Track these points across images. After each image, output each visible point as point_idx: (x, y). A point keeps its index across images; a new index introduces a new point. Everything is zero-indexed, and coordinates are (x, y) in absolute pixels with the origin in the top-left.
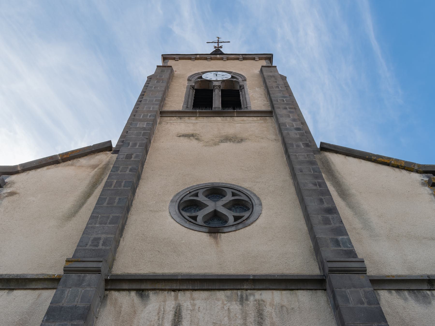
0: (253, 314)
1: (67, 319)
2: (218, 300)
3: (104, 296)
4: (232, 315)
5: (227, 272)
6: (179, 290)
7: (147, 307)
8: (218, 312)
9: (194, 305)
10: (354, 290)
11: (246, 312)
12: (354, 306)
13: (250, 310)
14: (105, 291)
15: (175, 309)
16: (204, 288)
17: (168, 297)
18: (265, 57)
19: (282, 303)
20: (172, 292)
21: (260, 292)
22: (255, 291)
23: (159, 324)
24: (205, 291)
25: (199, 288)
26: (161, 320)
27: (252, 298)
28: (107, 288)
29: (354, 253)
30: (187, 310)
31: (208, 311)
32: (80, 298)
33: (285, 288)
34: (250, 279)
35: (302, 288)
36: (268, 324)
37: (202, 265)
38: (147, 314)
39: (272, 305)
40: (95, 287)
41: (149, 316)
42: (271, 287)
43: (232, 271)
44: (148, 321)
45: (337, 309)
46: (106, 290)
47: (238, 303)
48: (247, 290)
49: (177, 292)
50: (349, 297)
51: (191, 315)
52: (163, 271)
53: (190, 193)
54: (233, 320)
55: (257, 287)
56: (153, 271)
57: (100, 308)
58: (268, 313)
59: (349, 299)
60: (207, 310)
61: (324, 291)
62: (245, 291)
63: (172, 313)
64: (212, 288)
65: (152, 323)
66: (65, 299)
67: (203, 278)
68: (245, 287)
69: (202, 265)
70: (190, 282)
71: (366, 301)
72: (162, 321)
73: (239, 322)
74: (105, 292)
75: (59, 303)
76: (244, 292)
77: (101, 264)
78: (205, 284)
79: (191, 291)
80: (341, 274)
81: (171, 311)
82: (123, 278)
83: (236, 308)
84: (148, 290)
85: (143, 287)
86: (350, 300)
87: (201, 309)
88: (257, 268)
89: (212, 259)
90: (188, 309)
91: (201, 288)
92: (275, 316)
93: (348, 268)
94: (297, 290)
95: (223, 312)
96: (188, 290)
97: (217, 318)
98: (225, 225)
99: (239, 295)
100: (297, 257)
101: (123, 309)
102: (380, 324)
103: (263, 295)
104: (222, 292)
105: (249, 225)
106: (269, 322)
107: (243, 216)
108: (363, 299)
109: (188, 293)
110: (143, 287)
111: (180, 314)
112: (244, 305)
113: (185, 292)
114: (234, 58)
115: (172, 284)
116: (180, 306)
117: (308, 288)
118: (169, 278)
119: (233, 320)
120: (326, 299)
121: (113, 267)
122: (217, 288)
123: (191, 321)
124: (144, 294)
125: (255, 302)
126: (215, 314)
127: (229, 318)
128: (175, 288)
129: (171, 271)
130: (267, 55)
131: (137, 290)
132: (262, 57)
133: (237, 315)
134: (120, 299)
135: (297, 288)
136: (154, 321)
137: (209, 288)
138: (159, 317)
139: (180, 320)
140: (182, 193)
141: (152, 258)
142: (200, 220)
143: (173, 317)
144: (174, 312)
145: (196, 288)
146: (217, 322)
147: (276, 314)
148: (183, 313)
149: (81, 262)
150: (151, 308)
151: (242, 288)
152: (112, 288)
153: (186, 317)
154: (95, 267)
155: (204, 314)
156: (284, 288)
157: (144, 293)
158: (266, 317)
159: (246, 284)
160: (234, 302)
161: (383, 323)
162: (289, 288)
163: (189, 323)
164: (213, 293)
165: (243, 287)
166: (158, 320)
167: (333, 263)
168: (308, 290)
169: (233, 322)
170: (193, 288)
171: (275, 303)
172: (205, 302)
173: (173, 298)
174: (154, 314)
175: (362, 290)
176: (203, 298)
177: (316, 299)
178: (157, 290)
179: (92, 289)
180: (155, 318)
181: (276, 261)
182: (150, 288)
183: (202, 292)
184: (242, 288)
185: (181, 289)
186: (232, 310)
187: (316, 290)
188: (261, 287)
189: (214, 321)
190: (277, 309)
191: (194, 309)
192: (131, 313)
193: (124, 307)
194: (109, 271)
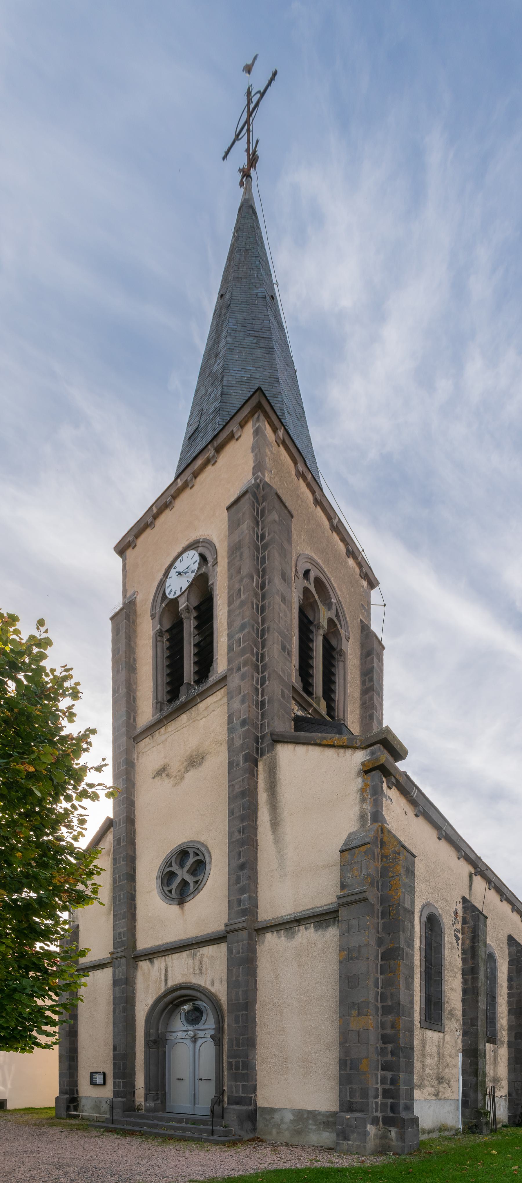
9: (173, 963)
18: (249, 413)
21: (202, 948)
27: (198, 954)
48: (196, 948)
53: (167, 863)
63: (164, 970)
98: (188, 894)
105: (202, 890)
107: (199, 880)
114: (202, 464)
127: (187, 969)
130: (250, 402)
132: (245, 417)
140: (162, 867)
142: (191, 854)
183: (176, 954)
194: (257, 689)
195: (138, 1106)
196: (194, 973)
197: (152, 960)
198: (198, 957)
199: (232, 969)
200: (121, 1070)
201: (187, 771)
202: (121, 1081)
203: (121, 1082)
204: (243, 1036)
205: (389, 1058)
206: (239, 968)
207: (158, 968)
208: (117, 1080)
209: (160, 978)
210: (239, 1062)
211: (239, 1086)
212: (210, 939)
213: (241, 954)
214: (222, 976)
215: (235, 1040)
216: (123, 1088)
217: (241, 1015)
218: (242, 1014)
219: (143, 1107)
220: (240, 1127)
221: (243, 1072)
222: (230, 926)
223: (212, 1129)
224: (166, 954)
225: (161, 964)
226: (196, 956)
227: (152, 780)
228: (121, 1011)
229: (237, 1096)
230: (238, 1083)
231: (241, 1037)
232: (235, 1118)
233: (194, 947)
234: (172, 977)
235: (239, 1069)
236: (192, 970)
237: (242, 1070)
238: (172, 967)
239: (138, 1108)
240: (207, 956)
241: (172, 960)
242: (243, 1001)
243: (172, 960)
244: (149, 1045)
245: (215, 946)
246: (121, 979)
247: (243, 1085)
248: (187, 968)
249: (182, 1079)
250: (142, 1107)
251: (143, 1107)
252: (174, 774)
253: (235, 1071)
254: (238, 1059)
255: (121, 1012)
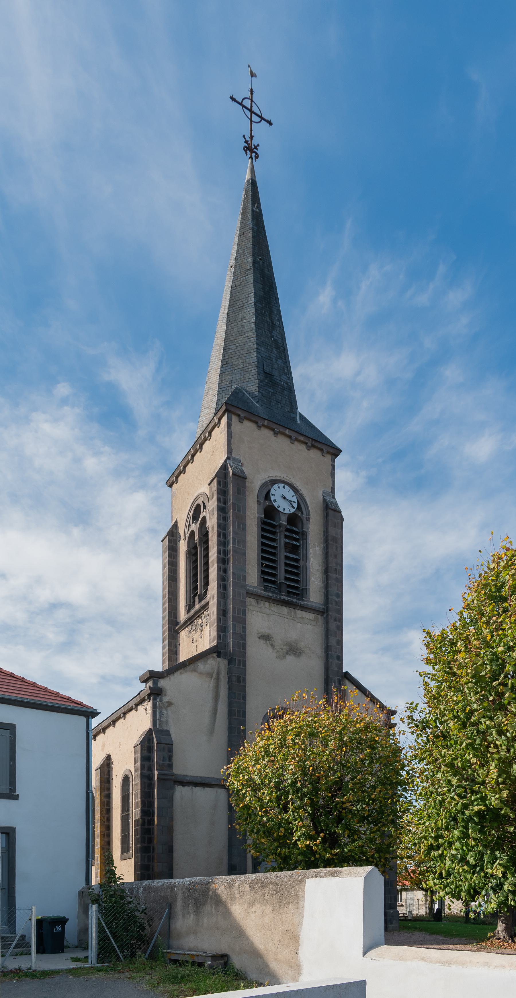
201: (287, 653)
205: (146, 827)
227: (258, 639)
252: (278, 648)
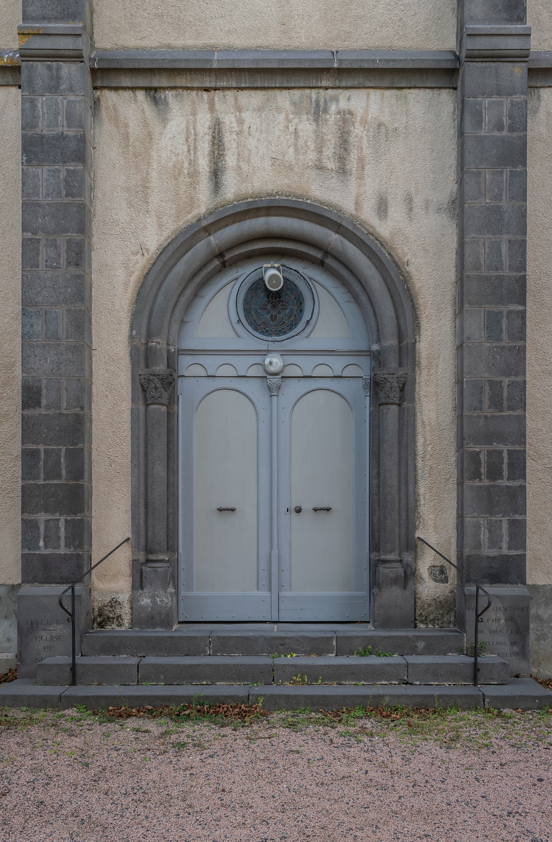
0: (333, 141)
1: (57, 161)
2: (279, 110)
3: (95, 103)
4: (301, 142)
5: (295, 44)
6: (216, 89)
7: (168, 126)
8: (279, 137)
9: (241, 122)
10: (496, 99)
11: (322, 137)
12: (487, 134)
13: (329, 133)
14: (94, 89)
15: (213, 131)
16: (256, 85)
17: (199, 105)
19: (381, 118)
20: (204, 92)
21: (347, 93)
22: (340, 91)
23: (190, 160)
24: (258, 91)
25: (247, 85)
26: (192, 152)
27: (333, 108)
28: (96, 85)
29: (524, 5)
30: (231, 132)
31: (264, 135)
32: (65, 118)
33: (390, 86)
34: (333, 69)
35: (417, 85)
36: (353, 160)
37: (251, 26)
38: (171, 141)
39: (364, 121)
40: (82, 94)
41: (173, 144)
42: (368, 84)
43: (304, 40)
44: (173, 155)
45: (461, 137)
46: (95, 88)
47: (311, 117)
48: (326, 88)
49: (213, 92)
50: (484, 116)
51: (237, 143)
52: (183, 42)
54: (302, 152)
55: (344, 84)
56: (166, 42)
57: (94, 128)
58: (356, 139)
59: (484, 119)
60: (261, 132)
61: (452, 90)
62: (323, 92)
63: (208, 138)
64: (270, 85)
65: (180, 158)
66: (41, 119)
67: (254, 67)
68: (324, 83)
69: (251, 26)
70: (233, 73)
71: (508, 124)
72: (195, 153)
73: (311, 157)
74: (94, 91)
75: (35, 128)
76: (322, 92)
77: (80, 40)
78: (259, 78)
79: (235, 91)
80: (484, 64)
81: (206, 134)
82: (120, 67)
83: (307, 128)
84: (164, 88)
85: (156, 82)
86: (484, 121)
87: (253, 130)
88: (347, 35)
89: (269, 9)
90: (232, 130)
91: (251, 85)
92: (367, 144)
93: (498, 51)
94: (410, 88)
95: (288, 137)
96: (229, 88)
97: (277, 148)
99: (313, 100)
100: (423, 3)
101: (130, 130)
102: (514, 169)
103: (352, 100)
104: (285, 92)
106: (356, 157)
108: (504, 119)
109: (230, 94)
110: (156, 82)
111: (220, 141)
112: (321, 123)
113: (225, 93)
115: (203, 78)
116: (219, 125)
117: (428, 86)
118: (197, 67)
119: (302, 152)
120: (452, 109)
121: (95, 31)
122: (277, 85)
123: (239, 155)
124: (159, 98)
125: (339, 116)
126: (275, 141)
127: (296, 150)
128: (208, 85)
129: (197, 41)
131: (147, 89)
133: (309, 144)
134: (122, 109)
135: (409, 86)
136: (183, 154)
137: (264, 85)
138: (189, 146)
139: (221, 153)
141: (160, 6)
143: (210, 146)
144: (211, 137)
145: (243, 85)
146: (277, 157)
147: (368, 141)
148: (226, 139)
149: (45, 37)
150: (174, 129)
151: (319, 86)
152: (105, 85)
153: (230, 146)
154: (71, 48)
155: (258, 140)
156: (387, 85)
157: (158, 95)
158: (352, 148)
159: (325, 77)
160: (305, 117)
161: (520, 167)
162: (395, 85)
163: (236, 157)
164: (270, 93)
165: (321, 83)
166: (188, 151)
167: (477, 38)
168: (427, 90)
169: (301, 157)
170: (239, 86)
171: (370, 117)
172: (258, 115)
173: (207, 106)
174: (180, 140)
175: (509, 100)
176: (255, 106)
177: (436, 108)
178: (179, 89)
179: (78, 99)
180: (184, 149)
181: (383, 16)
182: (167, 85)
183: (252, 92)
184: (319, 85)
185: (218, 87)
186: (301, 133)
187: (440, 88)
188: (350, 84)
189: (273, 155)
190: (372, 130)
191: (241, 131)
192: (144, 137)
193: (131, 125)
195: (100, 609)
196: (320, 167)
197: (162, 95)
198: (332, 118)
199: (480, 173)
200: (59, 476)
202: (63, 519)
203: (62, 524)
204: (513, 378)
206: (501, 173)
207: (183, 126)
208: (42, 517)
209: (193, 163)
210: (500, 452)
211: (501, 526)
212: (391, 65)
213: (505, 133)
214: (413, 190)
215: (487, 388)
216: (67, 545)
217: (505, 314)
218: (509, 312)
219: (125, 612)
220: (516, 649)
221: (511, 483)
222: (483, 38)
223: (475, 663)
224: (219, 84)
225: (194, 114)
226: (326, 111)
228: (64, 255)
229: (494, 558)
230: (498, 517)
231: (506, 381)
232: (503, 621)
233: (324, 83)
234: (239, 167)
235: (501, 476)
236: (312, 156)
237: (508, 479)
238: (239, 133)
239: (100, 615)
240: (364, 121)
241: (239, 109)
242: (514, 274)
243: (239, 109)
244: (144, 391)
245: (388, 93)
246: (62, 137)
247: (513, 523)
248: (296, 145)
249: (233, 510)
250: (118, 612)
251: (125, 612)
253: (486, 482)
254: (496, 446)
255: (63, 261)
